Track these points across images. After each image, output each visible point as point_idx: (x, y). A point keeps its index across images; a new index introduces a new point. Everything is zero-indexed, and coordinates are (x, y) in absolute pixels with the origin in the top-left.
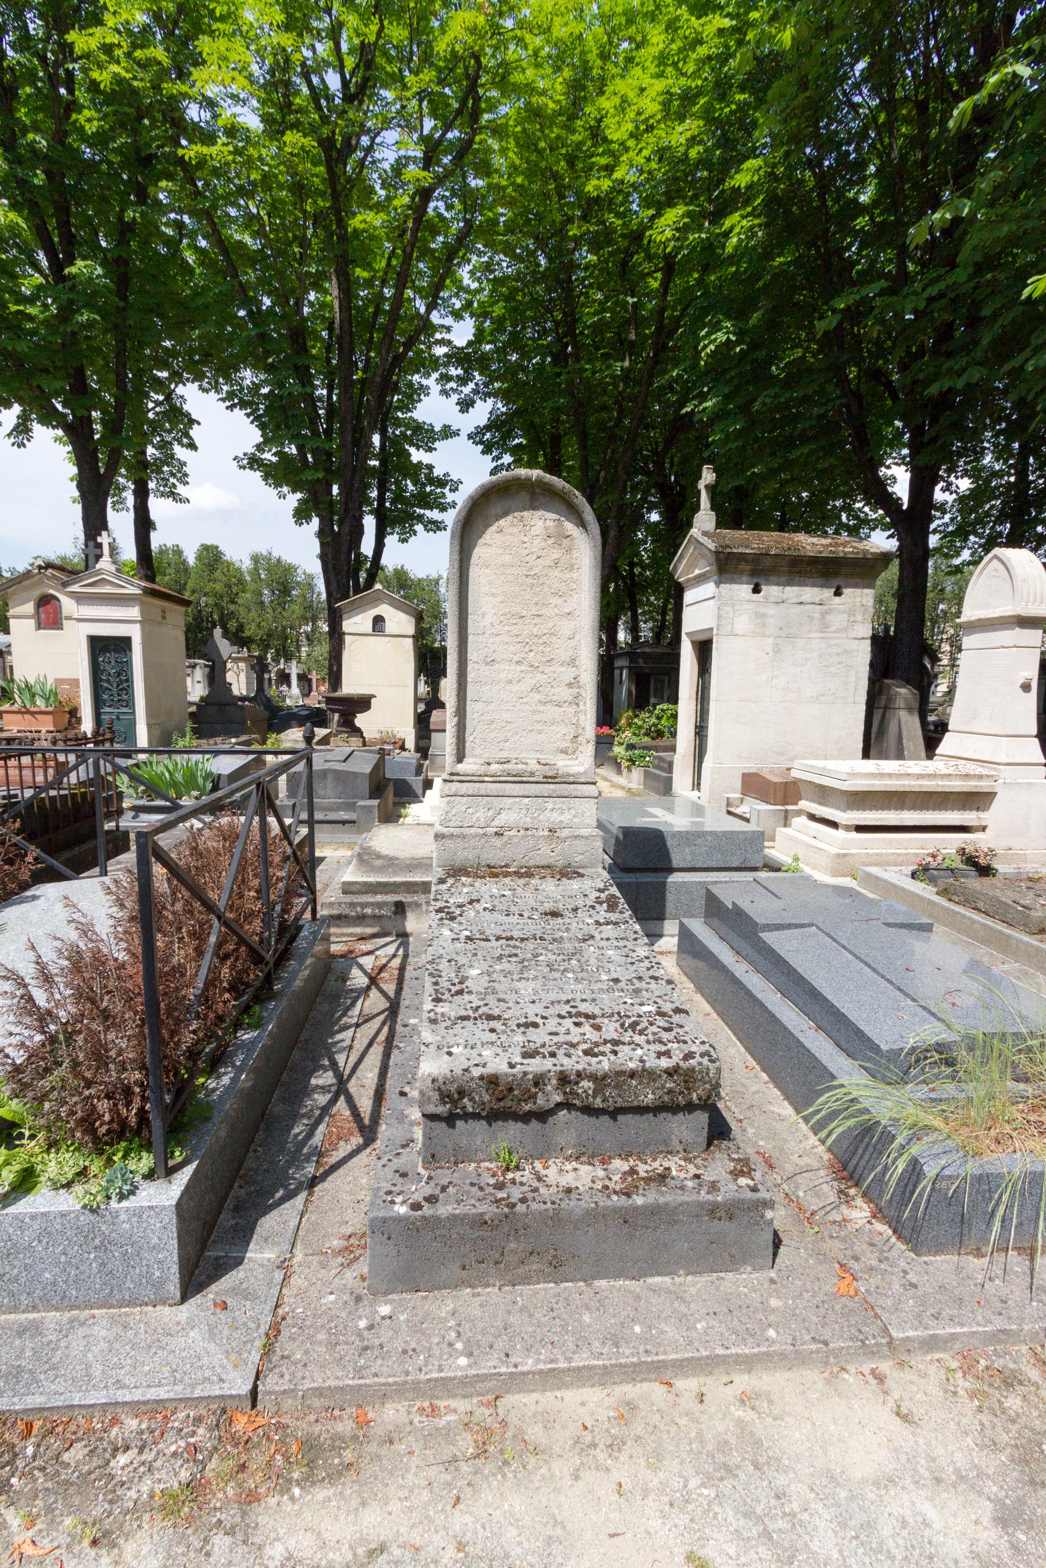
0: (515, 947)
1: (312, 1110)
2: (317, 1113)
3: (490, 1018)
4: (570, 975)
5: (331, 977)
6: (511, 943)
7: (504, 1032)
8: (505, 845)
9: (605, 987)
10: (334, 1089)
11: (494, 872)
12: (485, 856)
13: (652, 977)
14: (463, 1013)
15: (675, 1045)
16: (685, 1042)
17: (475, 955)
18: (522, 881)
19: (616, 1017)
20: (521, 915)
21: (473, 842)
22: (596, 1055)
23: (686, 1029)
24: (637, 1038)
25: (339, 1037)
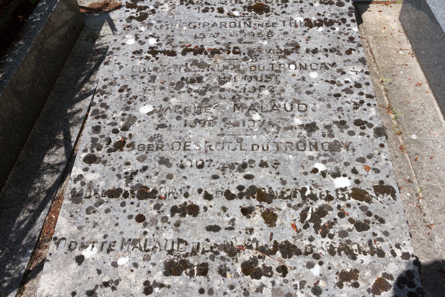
0: (202, 65)
1: (38, 194)
2: (43, 196)
3: (144, 193)
4: (256, 117)
5: (84, 35)
6: (200, 58)
7: (154, 221)
9: (295, 140)
10: (62, 168)
13: (358, 123)
14: (115, 184)
15: (367, 259)
16: (381, 254)
17: (153, 79)
19: (298, 200)
20: (221, 10)
22: (257, 275)
23: (388, 226)
24: (321, 244)
25: (78, 106)
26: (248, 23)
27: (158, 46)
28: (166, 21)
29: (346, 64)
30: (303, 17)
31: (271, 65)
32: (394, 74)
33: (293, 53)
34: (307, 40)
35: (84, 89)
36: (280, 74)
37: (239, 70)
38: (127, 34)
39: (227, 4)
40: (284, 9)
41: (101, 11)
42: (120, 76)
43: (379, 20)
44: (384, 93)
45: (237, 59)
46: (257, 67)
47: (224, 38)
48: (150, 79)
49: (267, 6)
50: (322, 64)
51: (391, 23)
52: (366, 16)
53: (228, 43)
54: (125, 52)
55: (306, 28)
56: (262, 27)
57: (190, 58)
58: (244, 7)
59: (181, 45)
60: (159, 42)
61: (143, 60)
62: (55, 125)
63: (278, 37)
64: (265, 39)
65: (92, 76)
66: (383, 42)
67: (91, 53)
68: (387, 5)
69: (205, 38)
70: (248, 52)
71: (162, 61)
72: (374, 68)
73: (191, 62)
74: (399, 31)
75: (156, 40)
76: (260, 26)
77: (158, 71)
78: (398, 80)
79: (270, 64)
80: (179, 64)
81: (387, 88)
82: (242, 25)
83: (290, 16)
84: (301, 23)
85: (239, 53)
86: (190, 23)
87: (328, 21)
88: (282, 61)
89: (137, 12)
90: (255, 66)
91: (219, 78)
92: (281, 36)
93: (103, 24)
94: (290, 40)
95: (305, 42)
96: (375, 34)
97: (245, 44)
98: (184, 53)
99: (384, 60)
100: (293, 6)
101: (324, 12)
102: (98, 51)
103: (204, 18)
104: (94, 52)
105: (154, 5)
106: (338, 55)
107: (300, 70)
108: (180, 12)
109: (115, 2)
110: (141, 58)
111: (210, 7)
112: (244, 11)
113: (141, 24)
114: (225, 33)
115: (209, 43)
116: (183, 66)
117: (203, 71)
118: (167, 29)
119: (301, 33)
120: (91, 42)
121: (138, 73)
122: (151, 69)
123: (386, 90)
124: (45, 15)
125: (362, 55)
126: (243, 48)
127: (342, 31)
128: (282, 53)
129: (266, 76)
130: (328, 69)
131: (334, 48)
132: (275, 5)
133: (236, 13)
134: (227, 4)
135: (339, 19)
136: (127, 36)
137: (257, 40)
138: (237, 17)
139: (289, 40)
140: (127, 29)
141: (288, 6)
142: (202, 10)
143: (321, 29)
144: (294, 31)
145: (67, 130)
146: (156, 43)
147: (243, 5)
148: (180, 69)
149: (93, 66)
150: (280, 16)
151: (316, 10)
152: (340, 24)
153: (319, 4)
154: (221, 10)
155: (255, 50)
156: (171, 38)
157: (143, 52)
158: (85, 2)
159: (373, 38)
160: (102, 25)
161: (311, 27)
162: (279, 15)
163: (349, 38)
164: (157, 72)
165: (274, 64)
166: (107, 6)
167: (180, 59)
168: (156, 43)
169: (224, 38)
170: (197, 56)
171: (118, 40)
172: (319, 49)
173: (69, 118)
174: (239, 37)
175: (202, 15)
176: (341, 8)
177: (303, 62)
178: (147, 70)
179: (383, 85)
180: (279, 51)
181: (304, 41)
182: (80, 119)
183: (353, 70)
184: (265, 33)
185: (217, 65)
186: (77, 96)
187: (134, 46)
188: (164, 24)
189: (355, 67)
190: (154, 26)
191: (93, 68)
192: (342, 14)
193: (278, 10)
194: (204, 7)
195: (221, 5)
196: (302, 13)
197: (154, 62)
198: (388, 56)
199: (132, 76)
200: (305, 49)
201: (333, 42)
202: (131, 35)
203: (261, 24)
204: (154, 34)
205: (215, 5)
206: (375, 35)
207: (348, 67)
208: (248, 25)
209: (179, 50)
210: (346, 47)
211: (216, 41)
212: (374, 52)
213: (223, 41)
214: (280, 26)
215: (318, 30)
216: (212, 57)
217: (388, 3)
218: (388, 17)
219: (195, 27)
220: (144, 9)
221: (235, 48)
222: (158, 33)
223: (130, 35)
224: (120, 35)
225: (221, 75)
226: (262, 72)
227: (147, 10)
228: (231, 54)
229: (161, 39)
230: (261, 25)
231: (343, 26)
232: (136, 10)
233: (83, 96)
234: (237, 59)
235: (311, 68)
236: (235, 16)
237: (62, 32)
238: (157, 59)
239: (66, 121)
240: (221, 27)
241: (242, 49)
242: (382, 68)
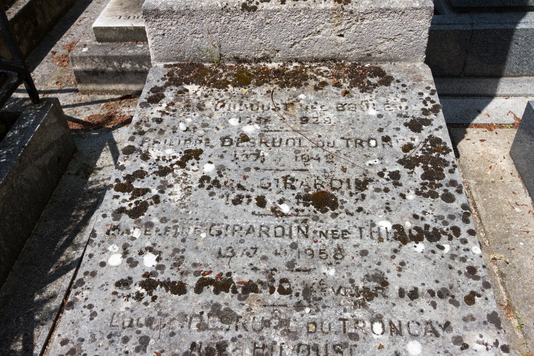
0: (227, 316)
5: (73, 167)
6: (226, 299)
8: (261, 25)
11: (246, 74)
12: (231, 44)
18: (283, 96)
20: (261, 202)
21: (207, 23)
25: (51, 289)
26: (304, 229)
27: (159, 271)
28: (175, 218)
29: (468, 325)
30: (391, 222)
31: (342, 322)
32: (511, 247)
33: (377, 296)
34: (400, 270)
35: (63, 258)
36: (357, 343)
37: (289, 331)
38: (111, 243)
39: (270, 190)
40: (360, 204)
41: (101, 127)
42: (89, 336)
43: (481, 154)
44: (499, 279)
45: (285, 306)
46: (319, 326)
47: (264, 258)
48: (138, 344)
49: (333, 196)
50: (427, 323)
51: (499, 160)
52: (462, 145)
53: (272, 270)
54: (103, 282)
55: (396, 244)
56: (326, 238)
57: (209, 300)
58: (298, 197)
59: (194, 270)
60: (161, 263)
61: (131, 300)
62: (13, 323)
63: (353, 261)
64: (331, 264)
65: (78, 236)
66: (490, 191)
67: (80, 196)
68: (491, 130)
69: (235, 258)
70: (303, 291)
71: (161, 304)
72: (481, 234)
73: (210, 309)
74: (511, 174)
75: (155, 257)
76: (323, 237)
77: (154, 326)
78: (517, 258)
79: (340, 319)
80: (189, 311)
81: (503, 269)
82: (295, 232)
83: (369, 218)
84: (387, 233)
85: (288, 292)
86: (213, 225)
87: (431, 230)
88: (359, 313)
89: (131, 199)
90: (314, 324)
91: (256, 348)
92: (358, 259)
93: (103, 148)
94: (372, 268)
95: (396, 273)
96: (477, 176)
97: (298, 274)
98: (199, 289)
99: (493, 222)
100: (373, 197)
101: (424, 213)
102: (91, 192)
103: (235, 217)
104: (85, 194)
105: (159, 187)
106: (452, 306)
107: (392, 335)
108: (198, 203)
109: (122, 115)
110: (129, 296)
111: (244, 193)
112: (298, 203)
113: (135, 223)
114: (266, 248)
115: (241, 271)
116: (196, 316)
117: (228, 330)
118: (175, 236)
119: (389, 254)
120: (82, 178)
121: (120, 328)
122: (142, 321)
123: (502, 275)
124: (14, 153)
125: (492, 307)
126: (296, 281)
127: (455, 252)
128: (359, 296)
129: (334, 347)
130: (437, 335)
131: (444, 289)
132: (346, 194)
133: (285, 208)
134: (270, 190)
135: (449, 227)
136: (110, 248)
137: (319, 266)
138: (287, 216)
139: (370, 267)
140: (111, 232)
141: (367, 198)
142: (233, 201)
143: (421, 247)
144: (378, 250)
145: (29, 334)
146: (155, 263)
147: (296, 192)
148: (190, 323)
149: (81, 218)
150: (355, 217)
151: (410, 207)
152: (450, 238)
153: (415, 196)
154: (261, 202)
155: (315, 287)
156: (180, 254)
157: (132, 282)
158: (82, 113)
159: (475, 183)
160: (101, 151)
161: (405, 242)
162: (352, 215)
163: (468, 268)
164: (151, 328)
165: (347, 320)
166: (111, 120)
167: (193, 302)
168: (155, 263)
169: (264, 258)
170: (219, 296)
171: (96, 255)
172: (420, 289)
173: (36, 310)
174: (289, 258)
175: (230, 210)
176: (449, 205)
177: (395, 318)
178: (135, 322)
179: (496, 265)
180: (354, 292)
181: (394, 272)
182: (51, 313)
183: (481, 339)
184: (331, 251)
185: (252, 318)
186: (51, 270)
187: (119, 269)
188: (172, 226)
189: (483, 333)
190: (154, 229)
191: (81, 222)
192: (452, 217)
193: (351, 204)
194: (235, 194)
195: (263, 190)
196: (388, 213)
197: (149, 306)
198: (499, 215)
199: (109, 337)
200: (397, 288)
201: (442, 275)
202: (118, 245)
203: (324, 232)
204: (154, 245)
205: (252, 190)
206: (479, 179)
207: (472, 332)
208: (303, 232)
209: (191, 281)
210: (464, 287)
211: (251, 264)
212: (479, 206)
213: (263, 266)
214: (354, 238)
215: (416, 249)
216: (245, 299)
217: (492, 128)
218: (494, 151)
219: (220, 233)
220: (143, 194)
221: (284, 281)
222: (161, 244)
223: (116, 247)
224: (99, 245)
225: (257, 340)
226: (326, 338)
227: (148, 196)
228: (276, 294)
229: (163, 256)
230: (324, 235)
231: (456, 241)
232: (130, 196)
233: (60, 270)
234: (285, 306)
235: (409, 333)
236: (283, 215)
237: (45, 160)
238: (154, 298)
239: (31, 315)
240: (260, 236)
241: (293, 283)
242: (492, 234)
